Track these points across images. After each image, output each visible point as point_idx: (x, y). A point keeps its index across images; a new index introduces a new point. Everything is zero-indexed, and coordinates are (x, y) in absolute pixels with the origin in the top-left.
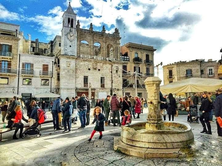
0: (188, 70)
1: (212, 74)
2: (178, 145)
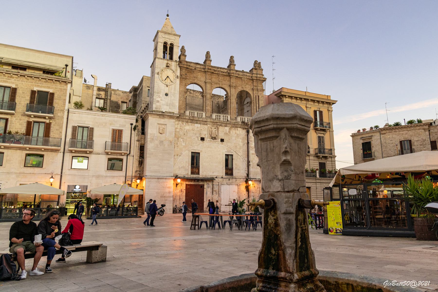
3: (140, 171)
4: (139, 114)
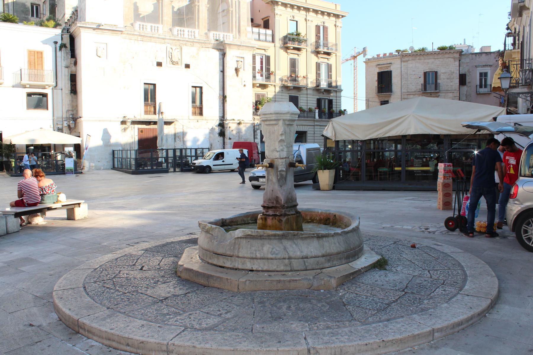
0: (429, 72)
2: (318, 262)
3: (72, 111)
4: (64, 26)
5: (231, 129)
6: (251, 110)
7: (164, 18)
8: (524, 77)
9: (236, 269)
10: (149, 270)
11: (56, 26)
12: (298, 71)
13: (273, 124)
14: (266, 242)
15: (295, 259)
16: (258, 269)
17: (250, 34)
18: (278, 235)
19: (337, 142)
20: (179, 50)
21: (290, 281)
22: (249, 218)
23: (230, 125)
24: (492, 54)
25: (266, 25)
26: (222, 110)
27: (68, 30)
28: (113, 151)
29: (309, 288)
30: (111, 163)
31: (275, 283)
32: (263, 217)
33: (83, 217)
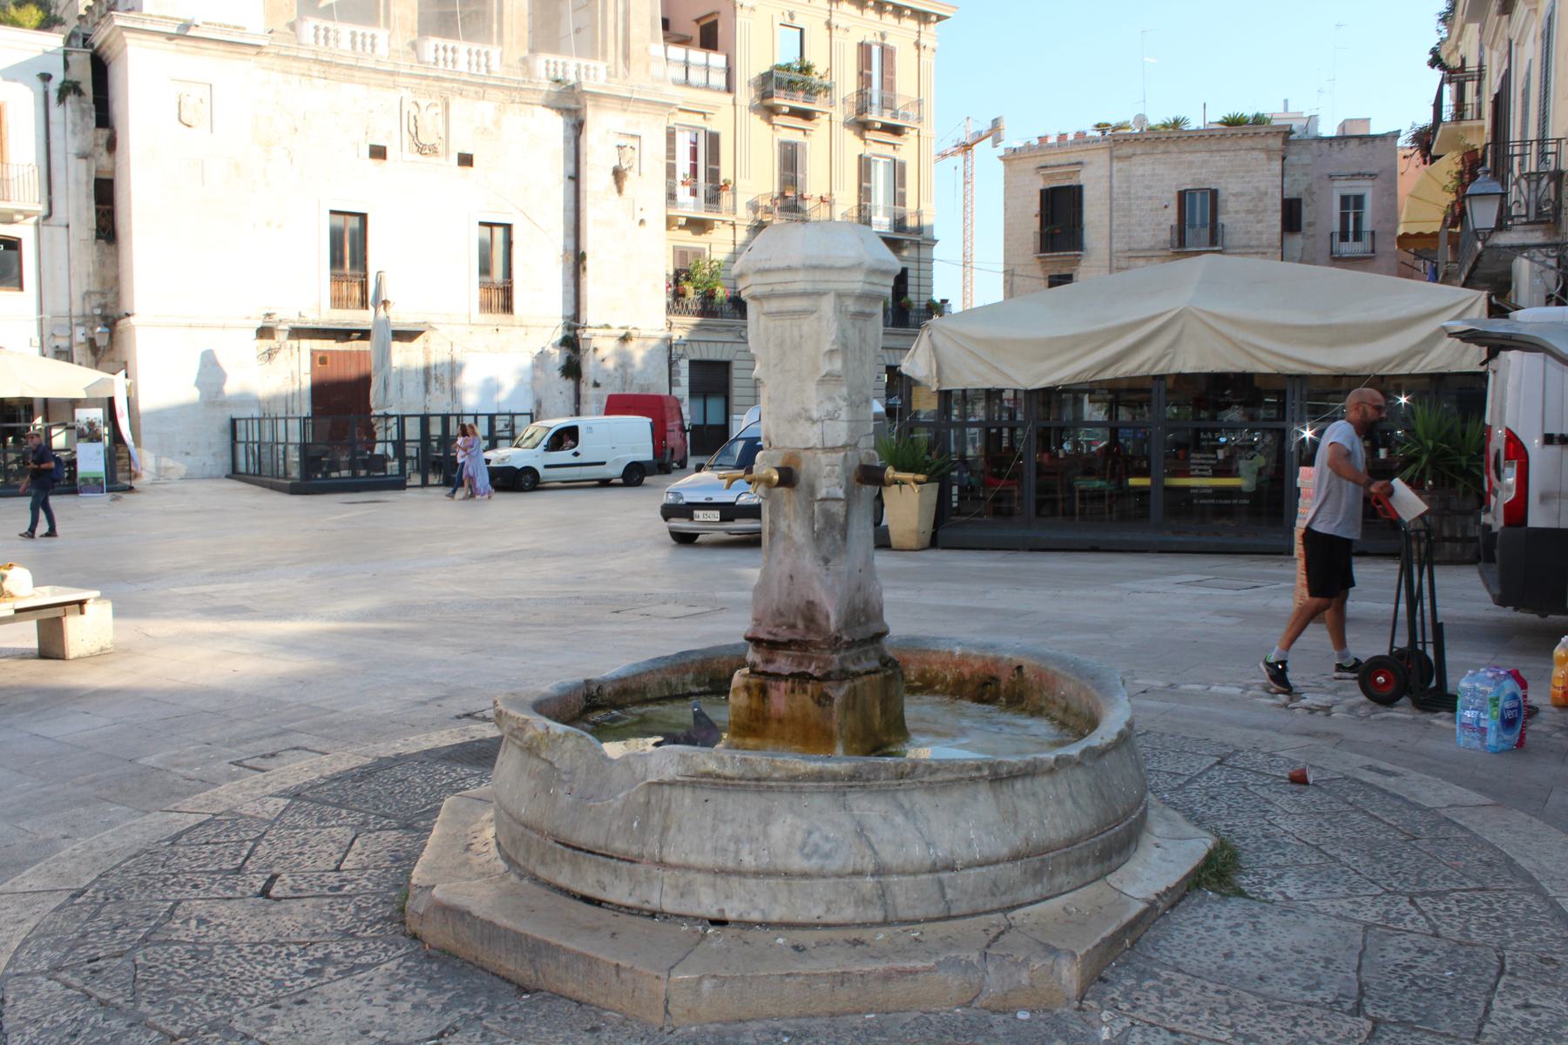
0: (1192, 192)
1: (1358, 237)
3: (103, 294)
4: (73, 24)
5: (600, 355)
6: (662, 297)
7: (392, 9)
8: (1532, 197)
9: (653, 915)
10: (297, 895)
11: (48, 24)
12: (804, 179)
13: (794, 312)
14: (780, 802)
15: (903, 873)
16: (747, 918)
17: (662, 65)
18: (835, 777)
19: (945, 396)
20: (440, 109)
21: (887, 977)
22: (689, 677)
23: (596, 343)
24: (1377, 142)
25: (709, 38)
26: (571, 297)
27: (85, 40)
28: (234, 422)
29: (969, 1004)
30: (227, 459)
31: (824, 986)
32: (753, 681)
33: (95, 648)
